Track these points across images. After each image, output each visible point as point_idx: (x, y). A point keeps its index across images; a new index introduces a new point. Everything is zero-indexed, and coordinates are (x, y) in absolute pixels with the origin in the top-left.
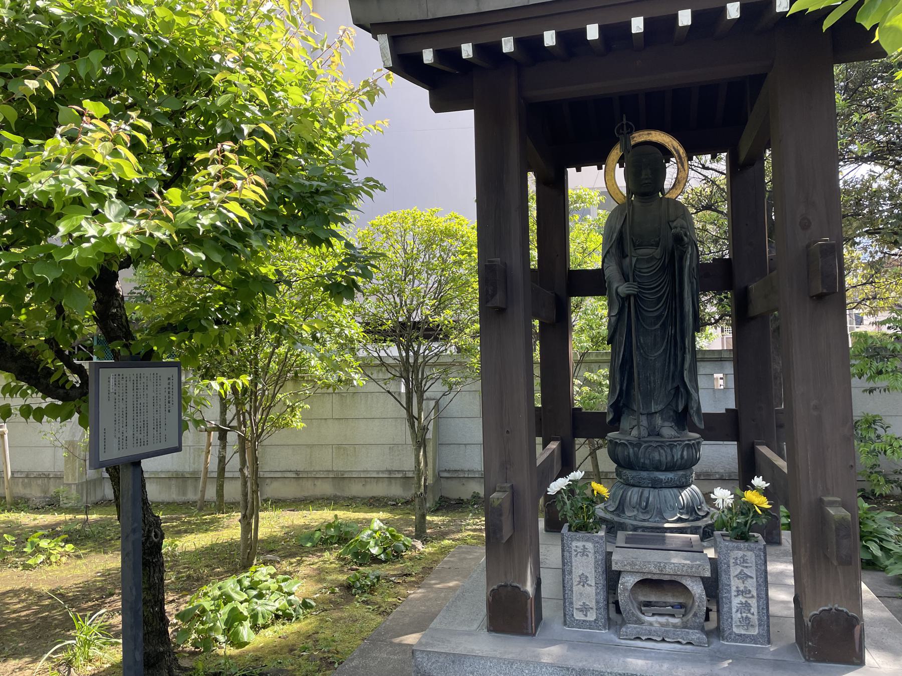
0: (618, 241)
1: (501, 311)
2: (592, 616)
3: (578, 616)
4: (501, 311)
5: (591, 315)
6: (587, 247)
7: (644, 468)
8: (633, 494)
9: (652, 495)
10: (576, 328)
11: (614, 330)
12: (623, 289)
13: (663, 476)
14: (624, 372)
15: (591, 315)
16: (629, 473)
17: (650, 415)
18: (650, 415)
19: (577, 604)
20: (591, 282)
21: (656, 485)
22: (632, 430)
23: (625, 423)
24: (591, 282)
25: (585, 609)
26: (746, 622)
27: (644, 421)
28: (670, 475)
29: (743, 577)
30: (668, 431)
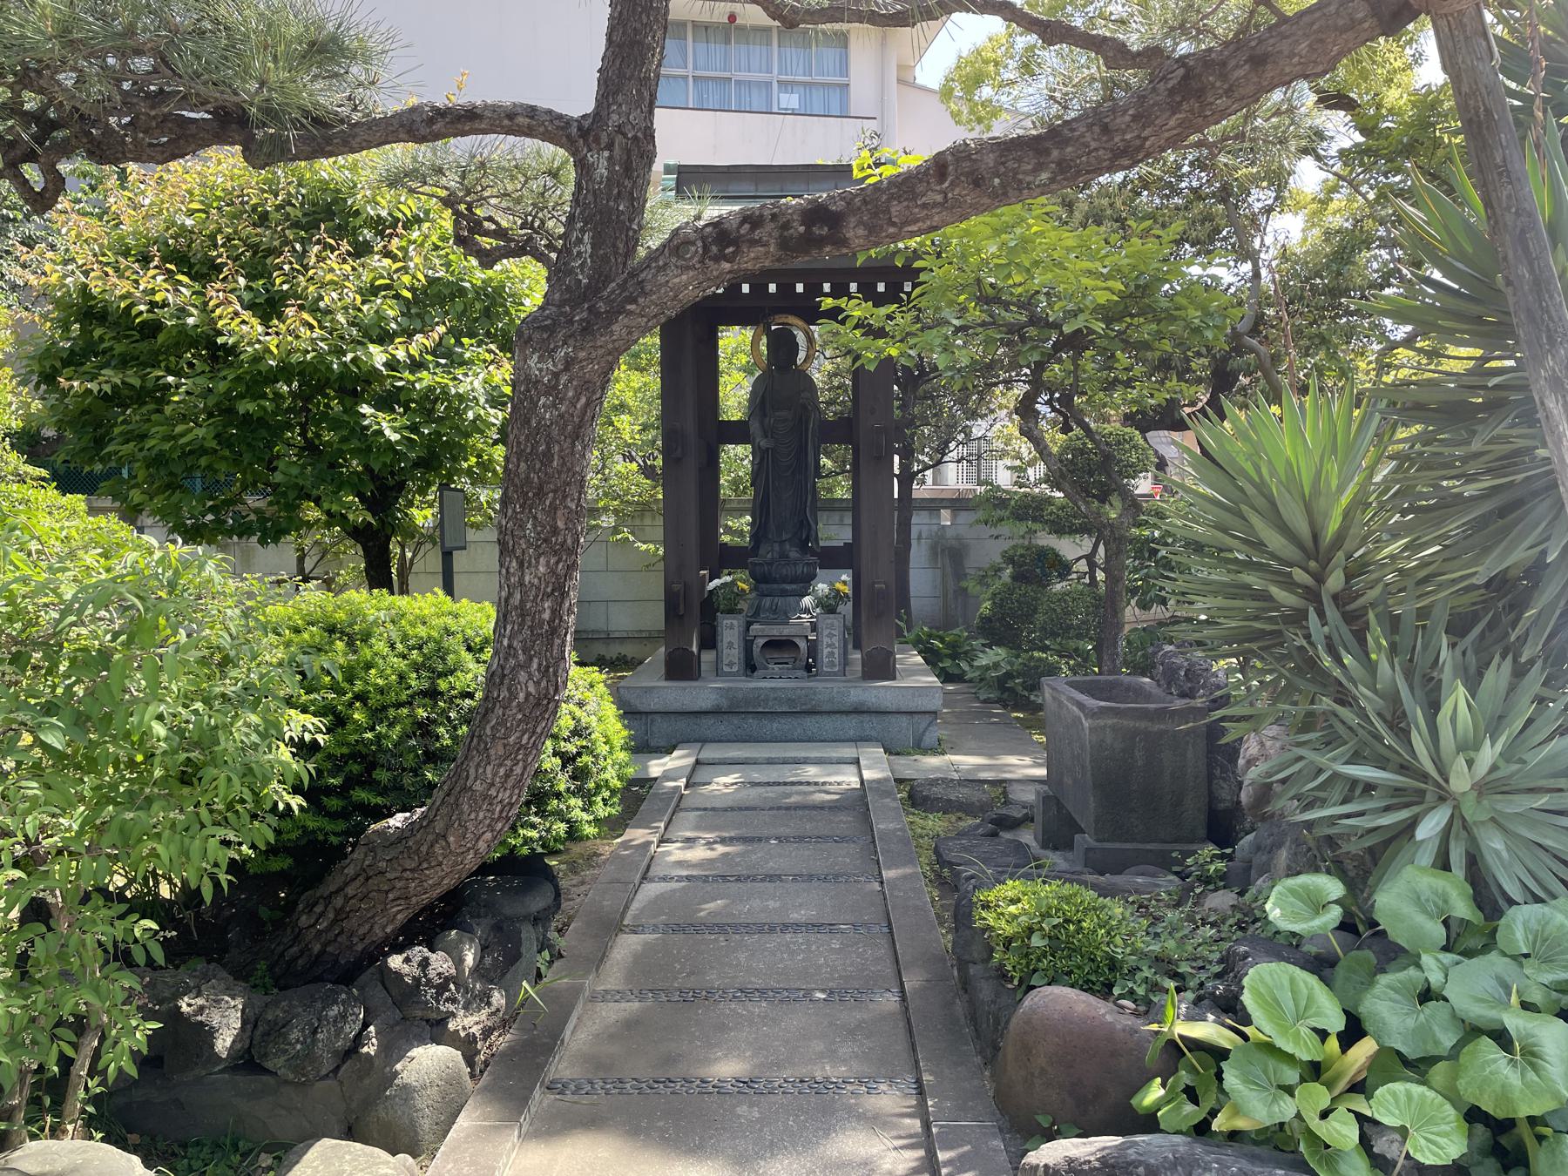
0: (761, 400)
1: (678, 460)
2: (735, 669)
3: (726, 669)
4: (678, 460)
5: (737, 459)
6: (735, 394)
7: (775, 581)
8: (767, 601)
9: (780, 601)
10: (59, 206)
11: (756, 476)
12: (763, 443)
13: (788, 587)
14: (761, 510)
15: (737, 459)
16: (763, 586)
17: (782, 542)
18: (782, 542)
19: (726, 661)
20: (736, 432)
21: (784, 594)
22: (768, 553)
23: (761, 551)
24: (736, 432)
25: (730, 664)
26: (832, 664)
27: (777, 547)
28: (794, 586)
29: (831, 636)
30: (794, 554)
